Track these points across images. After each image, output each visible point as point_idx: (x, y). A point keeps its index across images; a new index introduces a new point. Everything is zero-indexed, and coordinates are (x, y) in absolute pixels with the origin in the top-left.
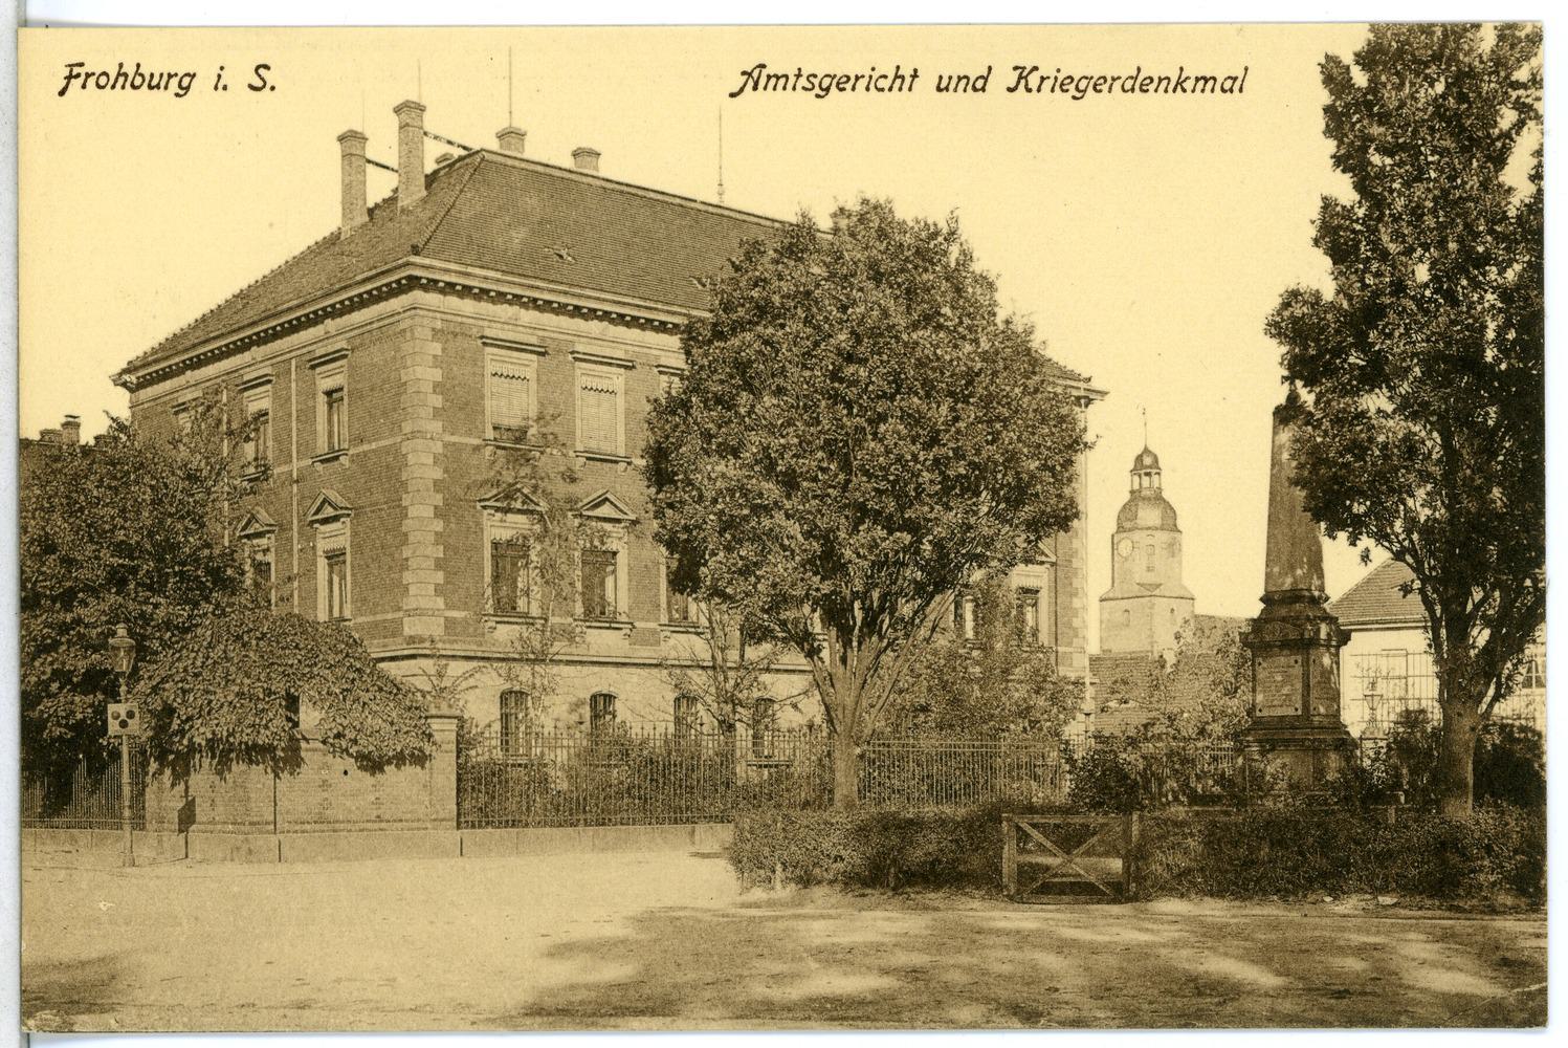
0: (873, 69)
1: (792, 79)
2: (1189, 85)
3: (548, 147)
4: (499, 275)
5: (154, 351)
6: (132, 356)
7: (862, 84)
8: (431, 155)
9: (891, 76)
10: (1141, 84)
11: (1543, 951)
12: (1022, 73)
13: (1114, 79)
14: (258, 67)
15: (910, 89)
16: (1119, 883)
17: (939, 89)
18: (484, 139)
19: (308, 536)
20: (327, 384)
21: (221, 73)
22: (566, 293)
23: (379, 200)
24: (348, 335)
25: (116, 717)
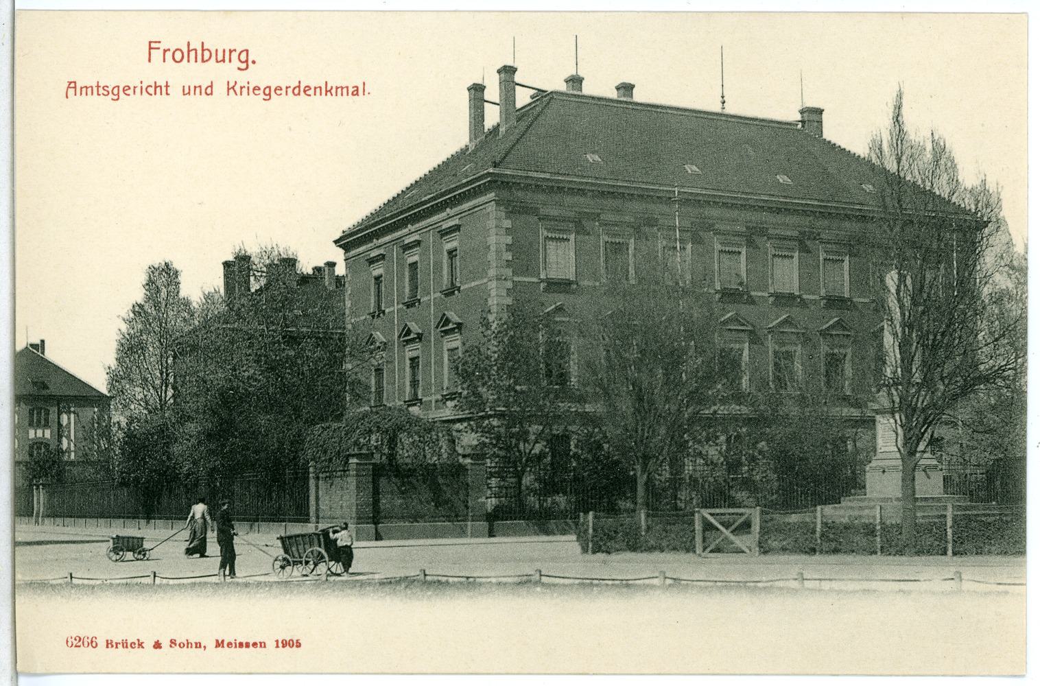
0: (141, 82)
1: (95, 89)
2: (333, 91)
3: (600, 85)
5: (359, 224)
6: (345, 228)
8: (523, 98)
10: (300, 90)
11: (467, 536)
13: (287, 88)
18: (555, 83)
19: (438, 342)
20: (449, 246)
23: (491, 127)
24: (459, 216)
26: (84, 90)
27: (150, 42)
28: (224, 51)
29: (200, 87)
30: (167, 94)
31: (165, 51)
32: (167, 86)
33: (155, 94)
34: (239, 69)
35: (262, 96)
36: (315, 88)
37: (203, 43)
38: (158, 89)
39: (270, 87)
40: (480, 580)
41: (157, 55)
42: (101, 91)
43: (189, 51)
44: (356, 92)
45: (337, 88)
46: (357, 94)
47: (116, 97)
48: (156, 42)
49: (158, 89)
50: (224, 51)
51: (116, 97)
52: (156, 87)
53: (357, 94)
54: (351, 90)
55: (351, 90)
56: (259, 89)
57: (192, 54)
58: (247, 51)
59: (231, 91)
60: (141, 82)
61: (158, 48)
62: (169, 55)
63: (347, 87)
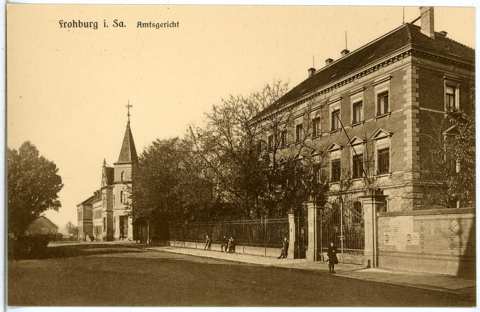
58: (97, 23)
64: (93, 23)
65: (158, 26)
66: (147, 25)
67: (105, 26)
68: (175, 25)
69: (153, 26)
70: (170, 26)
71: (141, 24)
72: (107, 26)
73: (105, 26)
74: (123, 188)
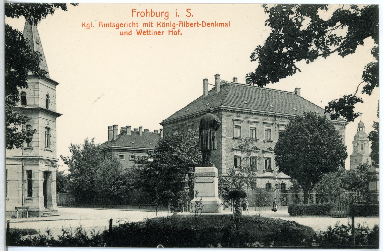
2: (218, 25)
4: (236, 108)
7: (196, 25)
9: (132, 23)
12: (100, 23)
14: (187, 9)
15: (229, 26)
16: (64, 232)
17: (121, 35)
21: (177, 11)
22: (248, 110)
25: (186, 189)
26: (106, 25)
27: (132, 10)
28: (159, 12)
29: (223, 23)
30: (137, 26)
31: (138, 13)
32: (137, 24)
33: (133, 26)
34: (165, 19)
35: (116, 27)
36: (211, 24)
37: (146, 10)
38: (134, 25)
39: (175, 24)
40: (342, 212)
41: (135, 14)
42: (112, 25)
43: (147, 13)
44: (227, 25)
45: (220, 24)
46: (227, 26)
47: (88, 28)
48: (134, 9)
49: (134, 25)
50: (159, 12)
51: (117, 28)
52: (133, 24)
53: (227, 26)
54: (225, 24)
55: (225, 24)
56: (193, 24)
57: (148, 14)
58: (168, 12)
59: (159, 25)
60: (171, 22)
61: (136, 12)
62: (139, 14)
63: (223, 23)
64: (140, 13)
65: (67, 220)
66: (146, 25)
67: (176, 16)
68: (138, 16)
69: (114, 26)
70: (129, 34)
71: (182, 24)
72: (179, 16)
73: (176, 16)
74: (275, 5)
